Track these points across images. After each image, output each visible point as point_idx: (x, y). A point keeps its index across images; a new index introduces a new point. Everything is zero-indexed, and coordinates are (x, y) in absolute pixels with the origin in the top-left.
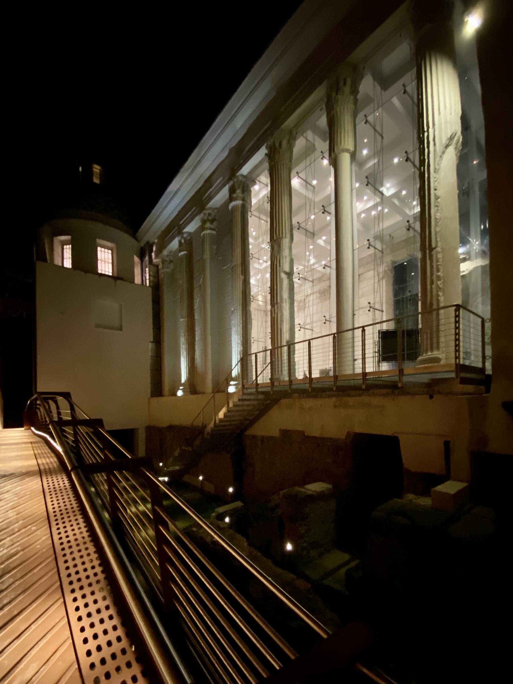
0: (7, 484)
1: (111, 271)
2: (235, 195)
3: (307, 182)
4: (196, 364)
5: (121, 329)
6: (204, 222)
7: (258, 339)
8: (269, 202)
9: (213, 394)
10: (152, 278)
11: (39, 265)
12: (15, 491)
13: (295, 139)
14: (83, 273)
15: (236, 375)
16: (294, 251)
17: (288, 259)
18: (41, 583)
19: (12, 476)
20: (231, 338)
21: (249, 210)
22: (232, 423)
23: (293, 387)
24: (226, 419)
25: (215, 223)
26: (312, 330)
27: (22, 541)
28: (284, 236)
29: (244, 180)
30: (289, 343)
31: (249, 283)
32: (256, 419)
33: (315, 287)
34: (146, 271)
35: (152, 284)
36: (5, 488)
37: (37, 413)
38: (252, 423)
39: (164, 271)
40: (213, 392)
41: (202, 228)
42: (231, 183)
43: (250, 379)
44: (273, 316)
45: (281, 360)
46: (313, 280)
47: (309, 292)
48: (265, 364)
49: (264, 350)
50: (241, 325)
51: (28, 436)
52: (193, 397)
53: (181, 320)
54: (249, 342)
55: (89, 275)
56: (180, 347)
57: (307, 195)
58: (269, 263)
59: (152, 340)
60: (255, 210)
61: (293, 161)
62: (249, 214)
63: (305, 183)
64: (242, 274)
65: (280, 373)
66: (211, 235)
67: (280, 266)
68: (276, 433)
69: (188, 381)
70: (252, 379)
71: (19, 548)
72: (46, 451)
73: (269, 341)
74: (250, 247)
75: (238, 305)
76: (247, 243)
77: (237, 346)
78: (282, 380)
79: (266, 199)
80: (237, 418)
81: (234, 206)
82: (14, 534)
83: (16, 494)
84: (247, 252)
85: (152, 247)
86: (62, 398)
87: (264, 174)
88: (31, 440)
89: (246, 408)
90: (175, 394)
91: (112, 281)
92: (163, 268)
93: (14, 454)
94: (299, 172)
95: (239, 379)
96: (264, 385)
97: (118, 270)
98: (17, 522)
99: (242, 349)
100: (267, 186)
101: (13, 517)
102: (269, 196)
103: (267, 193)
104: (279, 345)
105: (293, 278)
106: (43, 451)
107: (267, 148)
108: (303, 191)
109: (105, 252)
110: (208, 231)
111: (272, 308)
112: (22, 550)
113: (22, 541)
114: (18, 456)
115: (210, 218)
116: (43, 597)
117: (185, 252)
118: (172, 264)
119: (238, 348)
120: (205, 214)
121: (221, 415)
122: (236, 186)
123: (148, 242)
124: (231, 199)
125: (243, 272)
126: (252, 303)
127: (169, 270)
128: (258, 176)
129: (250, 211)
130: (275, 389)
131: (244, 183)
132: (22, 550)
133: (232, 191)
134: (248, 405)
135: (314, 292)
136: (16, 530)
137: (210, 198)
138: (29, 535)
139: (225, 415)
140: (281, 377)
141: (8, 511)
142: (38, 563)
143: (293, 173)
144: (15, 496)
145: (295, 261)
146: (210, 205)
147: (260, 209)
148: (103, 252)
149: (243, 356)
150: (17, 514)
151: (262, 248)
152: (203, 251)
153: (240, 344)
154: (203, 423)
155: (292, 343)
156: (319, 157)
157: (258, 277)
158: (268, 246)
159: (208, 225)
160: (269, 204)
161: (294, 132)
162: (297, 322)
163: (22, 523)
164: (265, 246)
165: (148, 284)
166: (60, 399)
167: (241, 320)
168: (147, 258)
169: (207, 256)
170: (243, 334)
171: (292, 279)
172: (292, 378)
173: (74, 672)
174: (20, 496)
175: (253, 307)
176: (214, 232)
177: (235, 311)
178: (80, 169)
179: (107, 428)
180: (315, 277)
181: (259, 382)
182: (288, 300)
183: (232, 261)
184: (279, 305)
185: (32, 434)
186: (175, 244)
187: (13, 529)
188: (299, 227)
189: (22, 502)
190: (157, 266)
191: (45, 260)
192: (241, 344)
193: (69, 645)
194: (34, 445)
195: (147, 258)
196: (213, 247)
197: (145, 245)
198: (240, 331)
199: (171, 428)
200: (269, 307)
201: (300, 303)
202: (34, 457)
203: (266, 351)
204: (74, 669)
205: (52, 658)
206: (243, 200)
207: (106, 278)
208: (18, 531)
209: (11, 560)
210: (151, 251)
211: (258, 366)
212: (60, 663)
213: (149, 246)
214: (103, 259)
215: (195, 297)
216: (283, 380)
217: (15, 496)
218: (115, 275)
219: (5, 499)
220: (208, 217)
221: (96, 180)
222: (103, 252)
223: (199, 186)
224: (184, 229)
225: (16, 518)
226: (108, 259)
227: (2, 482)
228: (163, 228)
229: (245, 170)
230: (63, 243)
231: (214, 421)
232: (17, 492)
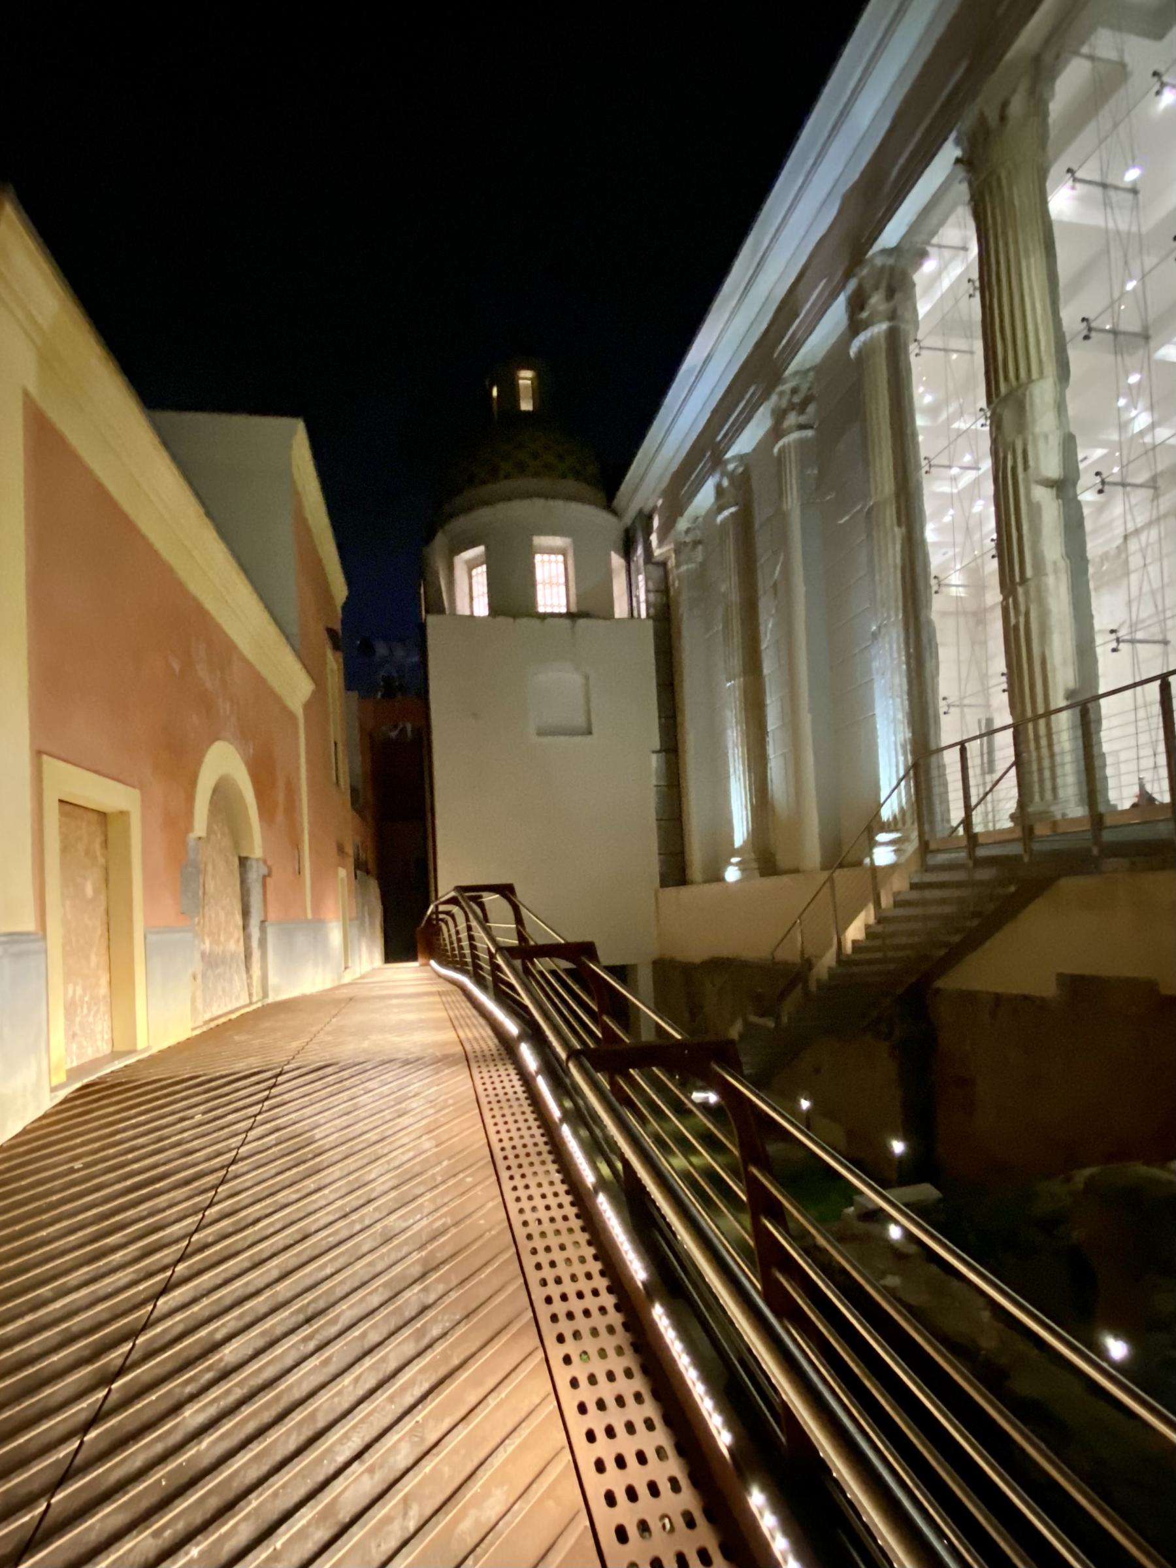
0: (412, 1079)
1: (564, 601)
2: (864, 315)
3: (1104, 186)
4: (772, 797)
5: (590, 733)
6: (779, 416)
7: (962, 699)
8: (978, 294)
9: (826, 874)
10: (652, 597)
11: (432, 621)
12: (429, 1095)
13: (1053, 77)
14: (511, 620)
15: (895, 817)
16: (1072, 409)
17: (1055, 441)
18: (495, 1307)
19: (420, 1062)
20: (873, 709)
21: (911, 338)
22: (890, 954)
23: (1107, 836)
24: (870, 943)
25: (811, 409)
26: (1165, 643)
27: (452, 1205)
28: (1035, 375)
29: (891, 261)
30: (1080, 698)
31: (923, 541)
32: (973, 940)
33: (1161, 500)
34: (637, 583)
35: (652, 611)
36: (412, 1087)
37: (440, 929)
38: (954, 956)
39: (680, 571)
40: (824, 867)
41: (776, 432)
42: (852, 285)
43: (942, 820)
44: (1013, 621)
45: (1052, 756)
46: (1154, 479)
47: (1140, 520)
48: (991, 770)
49: (983, 731)
50: (904, 667)
51: (427, 979)
52: (770, 882)
53: (729, 684)
54: (931, 712)
55: (524, 621)
56: (726, 754)
57: (1111, 225)
58: (987, 464)
59: (657, 747)
60: (930, 333)
61: (1050, 143)
62: (913, 348)
63: (1098, 191)
64: (899, 524)
65: (1049, 795)
66: (801, 443)
67: (1026, 467)
68: (1045, 987)
69: (753, 843)
70: (949, 821)
71: (449, 1221)
72: (470, 1014)
73: (1001, 700)
74: (921, 438)
75: (892, 613)
76: (909, 431)
77: (892, 730)
78: (1058, 816)
79: (966, 287)
80: (904, 940)
81: (865, 343)
82: (436, 1187)
83: (431, 1102)
84: (912, 457)
85: (650, 518)
86: (497, 896)
87: (952, 220)
88: (434, 989)
89: (933, 910)
90: (721, 879)
91: (566, 622)
92: (678, 565)
93: (412, 1017)
94: (1075, 167)
95: (904, 823)
96: (1000, 838)
97: (578, 596)
98: (440, 1163)
99: (909, 735)
100: (965, 249)
101: (430, 1149)
102: (975, 275)
103: (967, 269)
104: (1041, 710)
105: (1078, 492)
106: (463, 1013)
107: (958, 142)
108: (1096, 219)
109: (550, 562)
110: (795, 436)
111: (1005, 599)
112: (456, 1224)
113: (452, 1205)
114: (421, 1021)
115: (796, 400)
116: (504, 1338)
117: (733, 510)
118: (700, 547)
119: (895, 734)
120: (781, 394)
121: (855, 932)
122: (868, 286)
123: (640, 512)
124: (855, 326)
125: (903, 512)
126: (935, 596)
127: (692, 566)
128: (934, 233)
129: (916, 340)
130: (1036, 847)
131: (892, 269)
132: (456, 1224)
133: (857, 304)
134: (943, 901)
135: (1139, 525)
136: (439, 1179)
137: (795, 346)
138: (463, 1194)
139: (870, 932)
140: (1053, 808)
141: (421, 1136)
142: (483, 1261)
143: (1056, 170)
144: (428, 1105)
145: (1078, 441)
146: (793, 366)
147: (947, 324)
148: (546, 564)
149: (913, 759)
150: (437, 1146)
151: (960, 434)
152: (781, 494)
153: (903, 723)
154: (802, 952)
155: (1088, 695)
156: (1151, 89)
157: (947, 519)
158: (982, 421)
159: (792, 419)
160: (977, 301)
161: (1048, 58)
162: (1102, 621)
163: (447, 1166)
164: (968, 426)
165: (644, 615)
166: (489, 898)
167: (903, 653)
168: (640, 551)
169: (793, 503)
170: (910, 693)
171: (1076, 496)
172: (1102, 808)
173: (580, 1537)
174: (438, 1107)
175: (938, 607)
176: (809, 433)
177: (883, 631)
178: (495, 392)
179: (605, 960)
180: (1160, 468)
181: (978, 828)
182: (1063, 564)
183: (866, 496)
184: (1032, 585)
185: (433, 975)
186: (705, 497)
187: (433, 1176)
188: (1090, 329)
189: (443, 1120)
190: (663, 564)
191: (440, 610)
192: (906, 721)
193: (566, 1467)
194: (444, 999)
195: (640, 551)
196: (809, 472)
197: (634, 523)
198: (901, 685)
199: (717, 965)
200: (994, 596)
201: (1102, 565)
202: (449, 1024)
203: (991, 733)
204: (581, 1528)
205: (534, 1486)
206: (892, 316)
207: (556, 620)
208: (443, 1182)
209: (436, 1244)
210: (648, 531)
211: (972, 782)
212: (550, 1504)
213: (645, 519)
214: (547, 581)
215: (763, 617)
216: (1064, 815)
217: (428, 1105)
218: (574, 609)
219: (410, 1111)
220: (790, 401)
221: (526, 405)
222: (546, 564)
223: (764, 326)
224: (726, 452)
225: (436, 1154)
226: (558, 576)
227: (405, 1074)
228: (674, 467)
229: (891, 235)
230: (471, 565)
231: (834, 949)
232: (432, 1098)
